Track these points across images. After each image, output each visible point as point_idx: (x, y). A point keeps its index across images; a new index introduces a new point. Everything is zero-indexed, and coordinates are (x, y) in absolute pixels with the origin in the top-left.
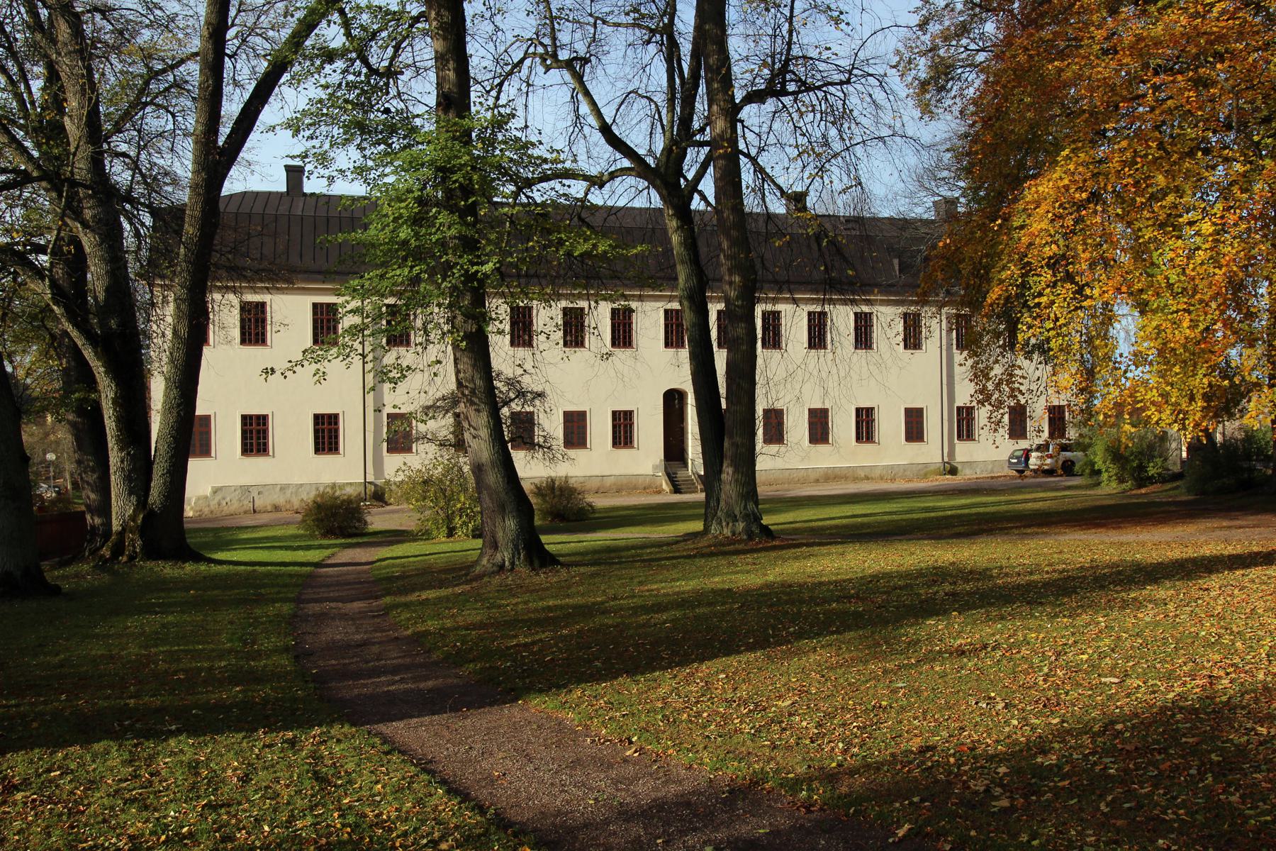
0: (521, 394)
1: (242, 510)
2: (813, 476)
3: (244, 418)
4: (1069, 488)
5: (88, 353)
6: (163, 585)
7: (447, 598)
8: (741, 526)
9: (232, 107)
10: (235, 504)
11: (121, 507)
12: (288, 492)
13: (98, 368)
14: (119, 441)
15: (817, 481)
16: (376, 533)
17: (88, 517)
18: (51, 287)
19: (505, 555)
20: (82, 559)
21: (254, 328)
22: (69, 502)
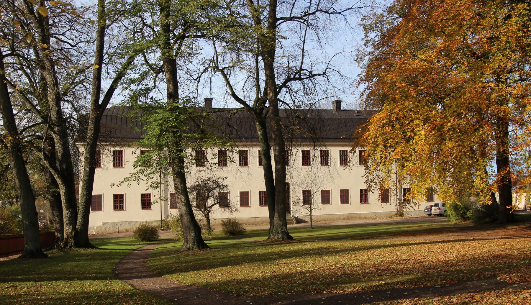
0: (219, 186)
1: (114, 231)
2: (342, 217)
3: (114, 195)
4: (441, 222)
5: (56, 177)
6: (81, 255)
7: (168, 258)
8: (280, 236)
9: (106, 85)
10: (111, 229)
11: (67, 229)
12: (132, 225)
13: (59, 181)
14: (66, 207)
15: (344, 219)
16: (162, 240)
17: (56, 233)
18: (44, 154)
19: (190, 245)
20: (54, 248)
21: (118, 160)
22: (48, 228)
